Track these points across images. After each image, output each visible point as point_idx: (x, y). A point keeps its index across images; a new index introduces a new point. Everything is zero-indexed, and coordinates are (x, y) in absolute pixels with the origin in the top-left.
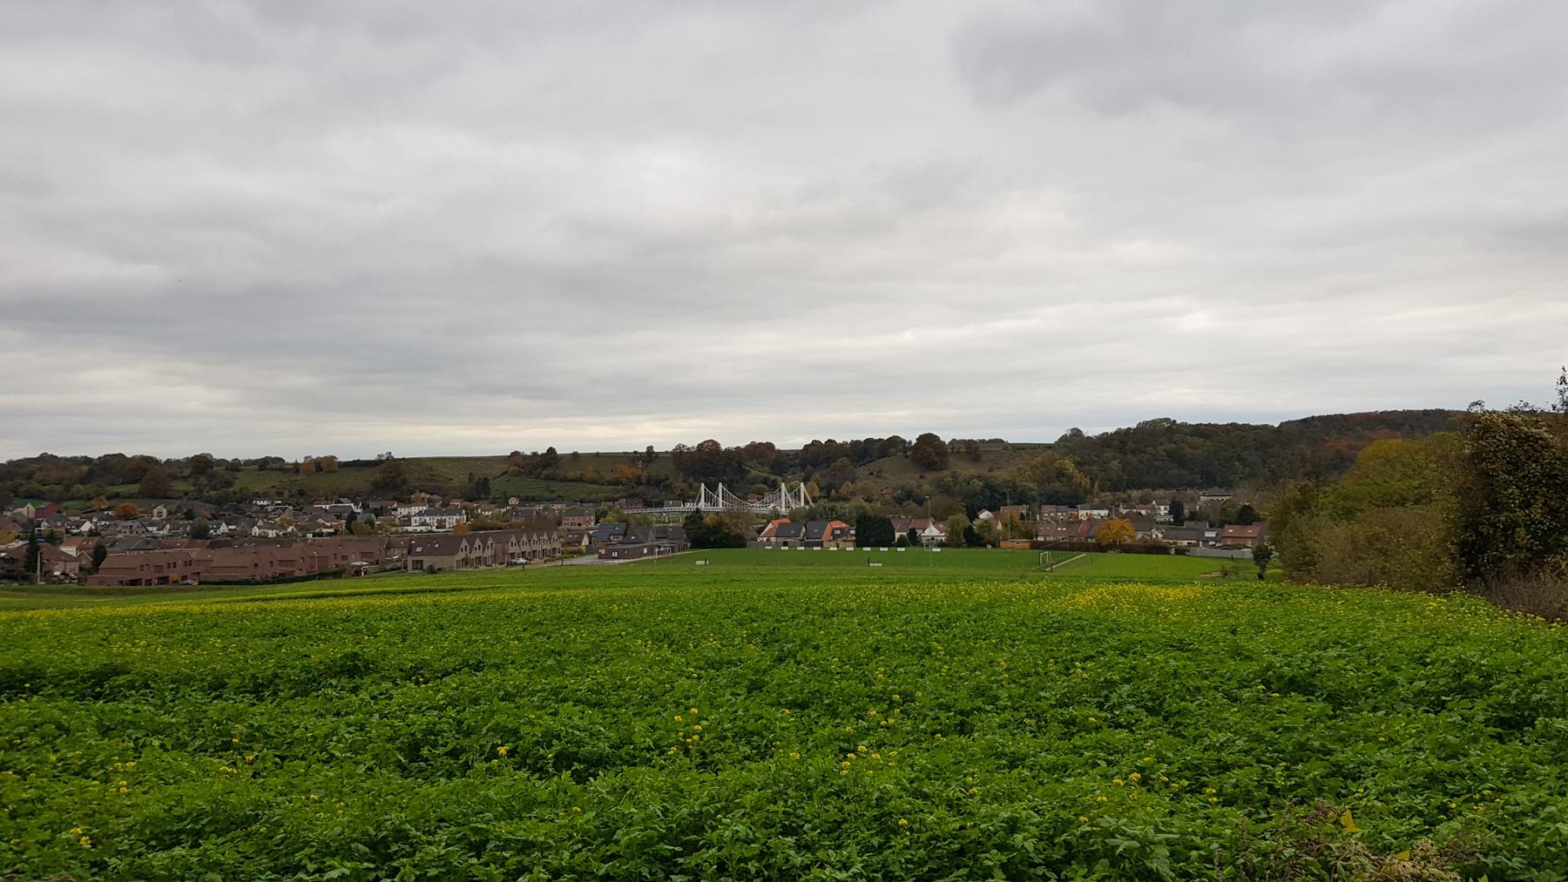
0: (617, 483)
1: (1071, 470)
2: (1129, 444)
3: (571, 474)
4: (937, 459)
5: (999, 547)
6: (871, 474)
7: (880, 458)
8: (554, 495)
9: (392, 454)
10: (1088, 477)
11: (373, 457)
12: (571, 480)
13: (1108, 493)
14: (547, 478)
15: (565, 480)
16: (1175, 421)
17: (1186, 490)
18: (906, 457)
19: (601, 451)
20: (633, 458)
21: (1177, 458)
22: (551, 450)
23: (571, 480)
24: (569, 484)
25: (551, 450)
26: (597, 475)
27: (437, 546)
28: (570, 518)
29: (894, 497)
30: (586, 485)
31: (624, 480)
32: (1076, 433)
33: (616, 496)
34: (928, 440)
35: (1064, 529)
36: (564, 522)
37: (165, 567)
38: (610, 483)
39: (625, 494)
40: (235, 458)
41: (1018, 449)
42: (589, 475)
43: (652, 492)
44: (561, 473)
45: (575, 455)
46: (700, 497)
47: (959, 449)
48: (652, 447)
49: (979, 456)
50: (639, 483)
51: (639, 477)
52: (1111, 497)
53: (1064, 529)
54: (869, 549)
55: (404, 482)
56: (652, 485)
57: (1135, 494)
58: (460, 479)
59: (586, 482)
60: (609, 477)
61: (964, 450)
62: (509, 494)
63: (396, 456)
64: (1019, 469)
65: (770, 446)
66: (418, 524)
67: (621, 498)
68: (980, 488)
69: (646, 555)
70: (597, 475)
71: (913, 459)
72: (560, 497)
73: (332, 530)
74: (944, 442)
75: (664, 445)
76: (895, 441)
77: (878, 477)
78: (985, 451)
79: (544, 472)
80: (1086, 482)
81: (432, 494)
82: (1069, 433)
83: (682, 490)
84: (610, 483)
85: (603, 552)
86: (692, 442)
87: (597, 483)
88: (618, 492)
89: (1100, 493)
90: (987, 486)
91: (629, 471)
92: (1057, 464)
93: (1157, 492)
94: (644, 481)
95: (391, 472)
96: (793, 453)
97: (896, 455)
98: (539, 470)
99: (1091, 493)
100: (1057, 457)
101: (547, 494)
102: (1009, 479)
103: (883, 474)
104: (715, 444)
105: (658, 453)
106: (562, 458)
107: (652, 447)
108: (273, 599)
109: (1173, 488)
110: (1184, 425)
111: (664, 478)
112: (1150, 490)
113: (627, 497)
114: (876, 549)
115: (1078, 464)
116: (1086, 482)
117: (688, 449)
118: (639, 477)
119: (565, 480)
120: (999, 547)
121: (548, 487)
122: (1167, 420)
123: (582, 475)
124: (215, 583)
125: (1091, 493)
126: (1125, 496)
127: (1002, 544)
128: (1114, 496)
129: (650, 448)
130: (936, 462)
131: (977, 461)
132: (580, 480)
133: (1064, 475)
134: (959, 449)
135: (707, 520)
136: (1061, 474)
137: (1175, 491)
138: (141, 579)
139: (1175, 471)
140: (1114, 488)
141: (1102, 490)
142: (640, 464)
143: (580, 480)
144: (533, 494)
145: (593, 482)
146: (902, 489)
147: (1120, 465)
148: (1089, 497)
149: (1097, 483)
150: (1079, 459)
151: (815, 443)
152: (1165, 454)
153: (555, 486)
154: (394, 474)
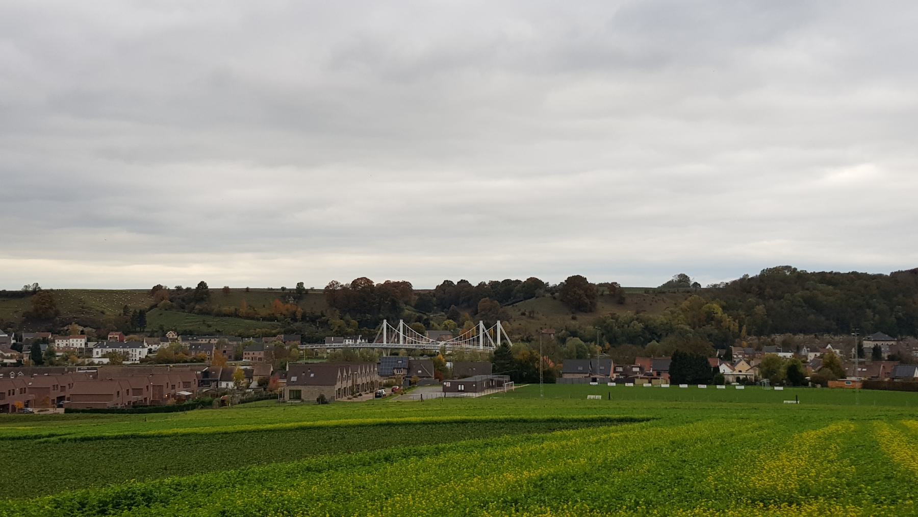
0: (271, 318)
1: (720, 314)
2: (768, 290)
3: (226, 309)
4: (587, 301)
5: (827, 386)
6: (523, 314)
7: (525, 299)
8: (211, 330)
9: (39, 286)
10: (737, 321)
11: (19, 288)
12: (225, 315)
13: (754, 337)
14: (201, 312)
15: (219, 315)
16: (795, 269)
17: (823, 335)
18: (554, 298)
19: (252, 286)
20: (283, 294)
21: (812, 303)
22: (202, 285)
23: (225, 315)
24: (224, 318)
25: (202, 285)
26: (252, 311)
27: (312, 375)
28: (251, 353)
29: (558, 337)
30: (242, 320)
31: (278, 315)
32: (684, 279)
33: (274, 331)
34: (576, 282)
35: (864, 370)
36: (244, 356)
37: (7, 393)
38: (264, 319)
39: (283, 330)
40: (158, 284)
41: (659, 293)
42: (243, 310)
43: (309, 329)
44: (215, 308)
45: (226, 290)
46: (382, 334)
47: (603, 291)
48: (302, 284)
49: (624, 299)
50: (295, 320)
51: (294, 313)
52: (756, 341)
53: (864, 370)
54: (686, 386)
55: (57, 313)
56: (308, 322)
57: (778, 338)
58: (112, 312)
59: (241, 317)
60: (264, 312)
61: (608, 293)
62: (165, 328)
63: (44, 287)
64: (672, 312)
65: (407, 285)
66: (100, 355)
67: (278, 333)
68: (640, 330)
69: (461, 391)
70: (252, 311)
71: (561, 300)
72: (219, 331)
73: (14, 361)
74: (543, 283)
75: (317, 282)
76: (534, 285)
77: (530, 317)
78: (629, 294)
79: (197, 307)
80: (734, 326)
81: (85, 326)
82: (676, 279)
83: (339, 327)
84: (264, 319)
85: (448, 384)
86: (346, 280)
87: (253, 319)
88: (274, 328)
89: (747, 336)
90: (646, 327)
91: (283, 308)
92: (705, 308)
93: (797, 337)
94: (299, 316)
95: (44, 304)
96: (428, 292)
97: (543, 296)
98: (192, 304)
99: (739, 336)
100: (704, 301)
101: (204, 329)
102: (665, 321)
103: (535, 315)
104: (368, 281)
105: (307, 290)
106: (212, 292)
107: (302, 284)
108: (552, 424)
109: (811, 333)
110: (813, 274)
111: (320, 314)
112: (791, 334)
113: (285, 333)
114: (712, 386)
115: (724, 308)
116: (734, 326)
117: (341, 286)
118: (294, 313)
119: (219, 315)
120: (827, 386)
121: (204, 321)
122: (788, 268)
123: (236, 309)
124: (83, 411)
125: (739, 336)
126: (769, 340)
127: (830, 383)
128: (759, 339)
129: (300, 285)
130: (587, 304)
131: (622, 303)
132: (236, 315)
133: (712, 319)
134: (603, 291)
135: (517, 357)
136: (710, 317)
137: (813, 336)
138: (8, 404)
139: (812, 317)
140: (759, 333)
141: (749, 334)
142: (291, 300)
143: (236, 315)
144: (191, 328)
145: (248, 318)
146: (566, 329)
147: (765, 310)
148: (737, 340)
149: (744, 328)
150: (724, 304)
151: (448, 284)
152: (801, 300)
153: (210, 320)
154: (47, 305)
